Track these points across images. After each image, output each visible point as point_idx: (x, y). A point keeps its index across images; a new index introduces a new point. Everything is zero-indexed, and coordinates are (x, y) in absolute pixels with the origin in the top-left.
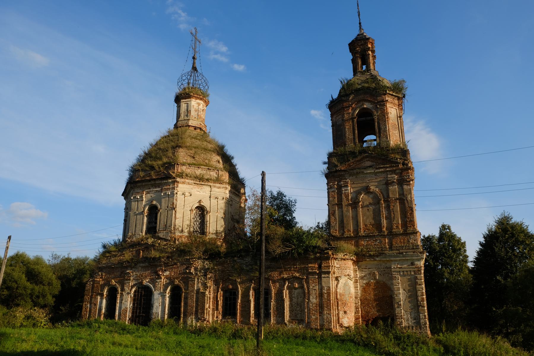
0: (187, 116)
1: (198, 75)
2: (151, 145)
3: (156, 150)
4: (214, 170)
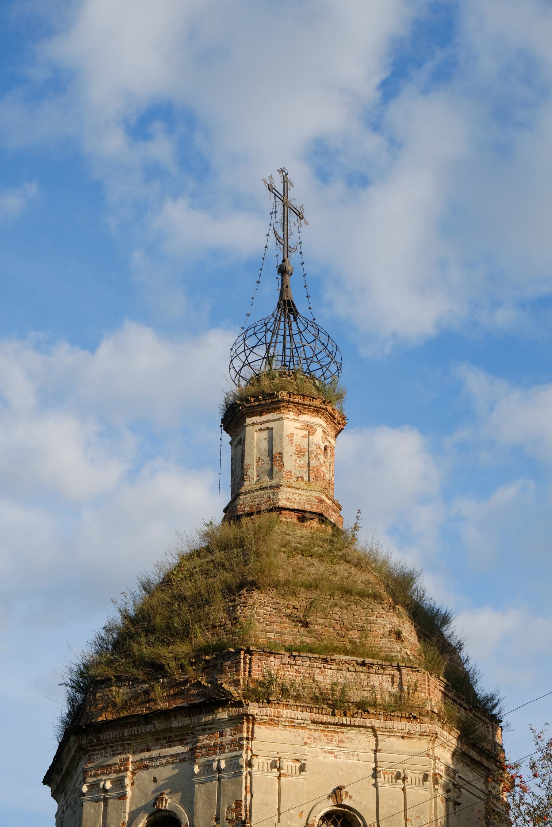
0: (270, 474)
1: (302, 328)
2: (146, 587)
3: (169, 604)
4: (382, 667)
